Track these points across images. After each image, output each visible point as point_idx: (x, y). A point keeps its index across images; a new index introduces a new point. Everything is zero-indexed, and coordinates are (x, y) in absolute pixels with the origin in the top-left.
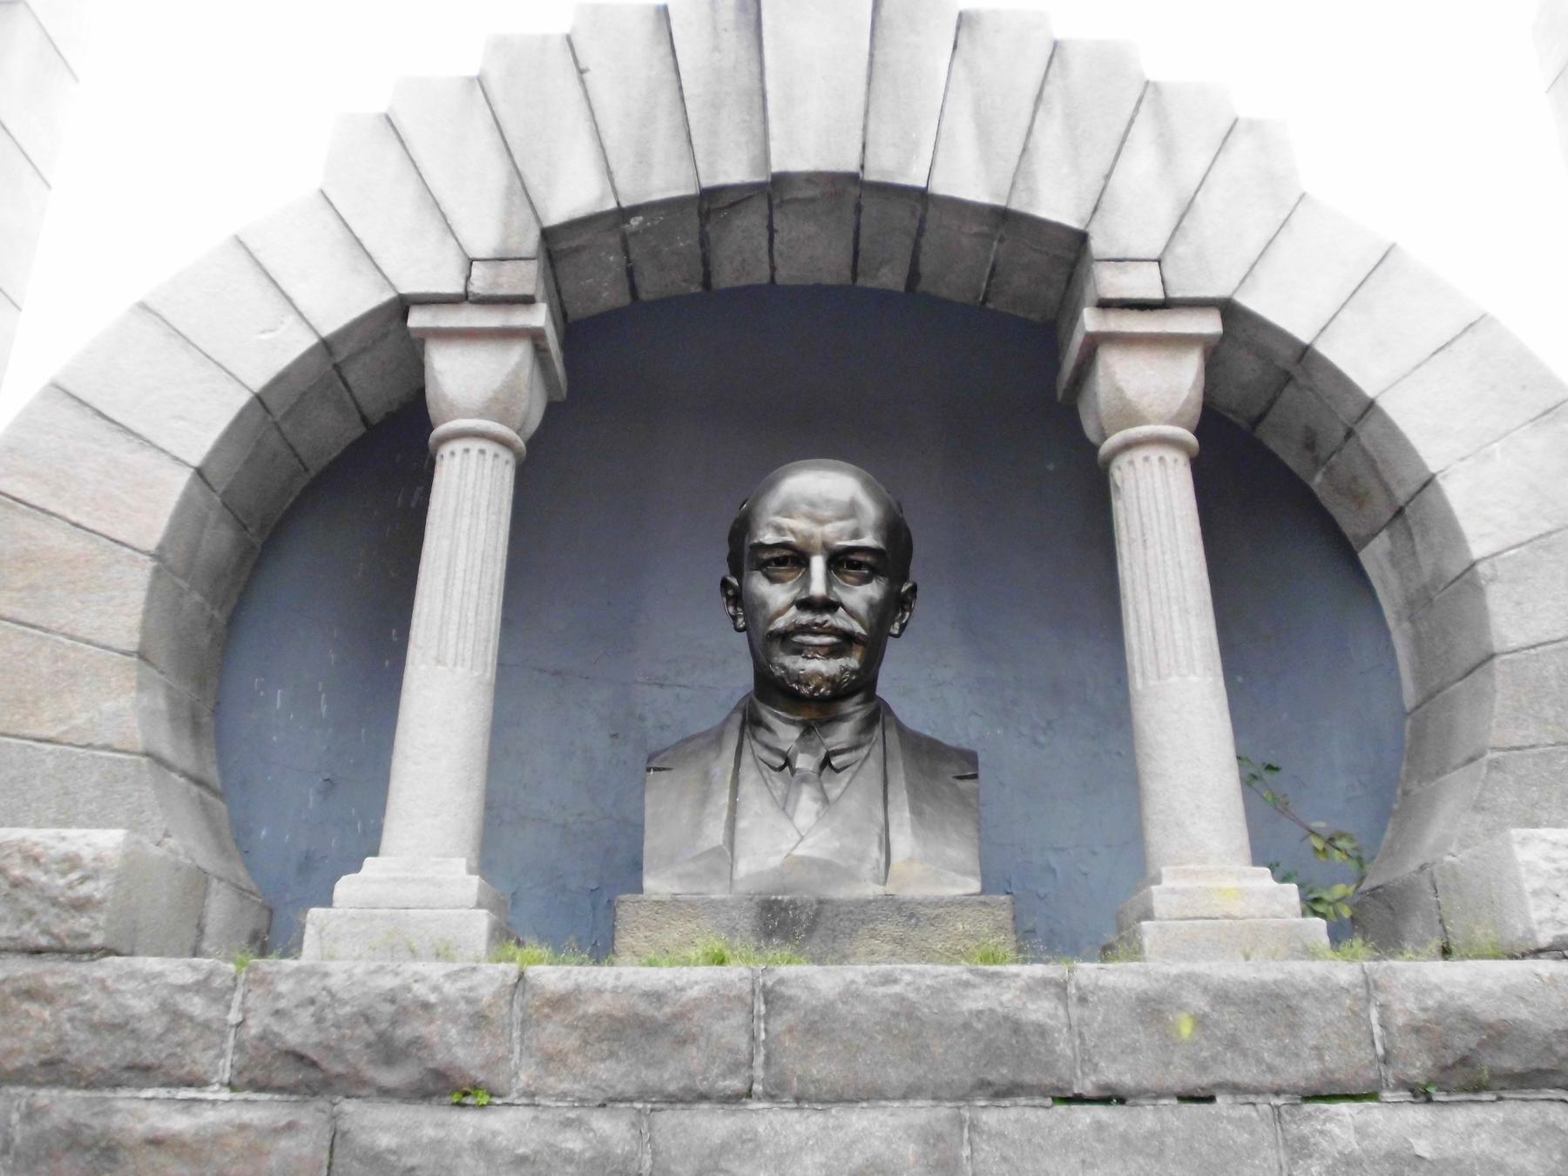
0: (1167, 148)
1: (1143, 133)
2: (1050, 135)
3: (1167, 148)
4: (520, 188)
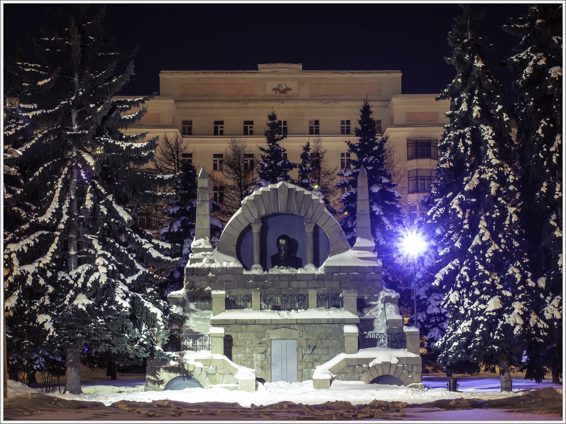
0: (313, 208)
1: (311, 206)
2: (303, 206)
3: (313, 208)
4: (259, 213)
